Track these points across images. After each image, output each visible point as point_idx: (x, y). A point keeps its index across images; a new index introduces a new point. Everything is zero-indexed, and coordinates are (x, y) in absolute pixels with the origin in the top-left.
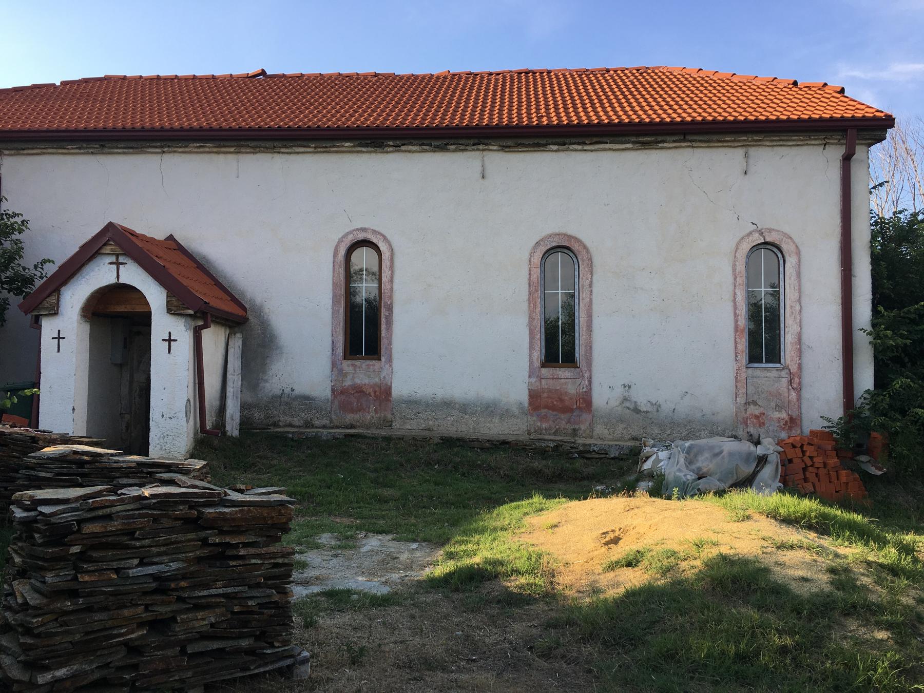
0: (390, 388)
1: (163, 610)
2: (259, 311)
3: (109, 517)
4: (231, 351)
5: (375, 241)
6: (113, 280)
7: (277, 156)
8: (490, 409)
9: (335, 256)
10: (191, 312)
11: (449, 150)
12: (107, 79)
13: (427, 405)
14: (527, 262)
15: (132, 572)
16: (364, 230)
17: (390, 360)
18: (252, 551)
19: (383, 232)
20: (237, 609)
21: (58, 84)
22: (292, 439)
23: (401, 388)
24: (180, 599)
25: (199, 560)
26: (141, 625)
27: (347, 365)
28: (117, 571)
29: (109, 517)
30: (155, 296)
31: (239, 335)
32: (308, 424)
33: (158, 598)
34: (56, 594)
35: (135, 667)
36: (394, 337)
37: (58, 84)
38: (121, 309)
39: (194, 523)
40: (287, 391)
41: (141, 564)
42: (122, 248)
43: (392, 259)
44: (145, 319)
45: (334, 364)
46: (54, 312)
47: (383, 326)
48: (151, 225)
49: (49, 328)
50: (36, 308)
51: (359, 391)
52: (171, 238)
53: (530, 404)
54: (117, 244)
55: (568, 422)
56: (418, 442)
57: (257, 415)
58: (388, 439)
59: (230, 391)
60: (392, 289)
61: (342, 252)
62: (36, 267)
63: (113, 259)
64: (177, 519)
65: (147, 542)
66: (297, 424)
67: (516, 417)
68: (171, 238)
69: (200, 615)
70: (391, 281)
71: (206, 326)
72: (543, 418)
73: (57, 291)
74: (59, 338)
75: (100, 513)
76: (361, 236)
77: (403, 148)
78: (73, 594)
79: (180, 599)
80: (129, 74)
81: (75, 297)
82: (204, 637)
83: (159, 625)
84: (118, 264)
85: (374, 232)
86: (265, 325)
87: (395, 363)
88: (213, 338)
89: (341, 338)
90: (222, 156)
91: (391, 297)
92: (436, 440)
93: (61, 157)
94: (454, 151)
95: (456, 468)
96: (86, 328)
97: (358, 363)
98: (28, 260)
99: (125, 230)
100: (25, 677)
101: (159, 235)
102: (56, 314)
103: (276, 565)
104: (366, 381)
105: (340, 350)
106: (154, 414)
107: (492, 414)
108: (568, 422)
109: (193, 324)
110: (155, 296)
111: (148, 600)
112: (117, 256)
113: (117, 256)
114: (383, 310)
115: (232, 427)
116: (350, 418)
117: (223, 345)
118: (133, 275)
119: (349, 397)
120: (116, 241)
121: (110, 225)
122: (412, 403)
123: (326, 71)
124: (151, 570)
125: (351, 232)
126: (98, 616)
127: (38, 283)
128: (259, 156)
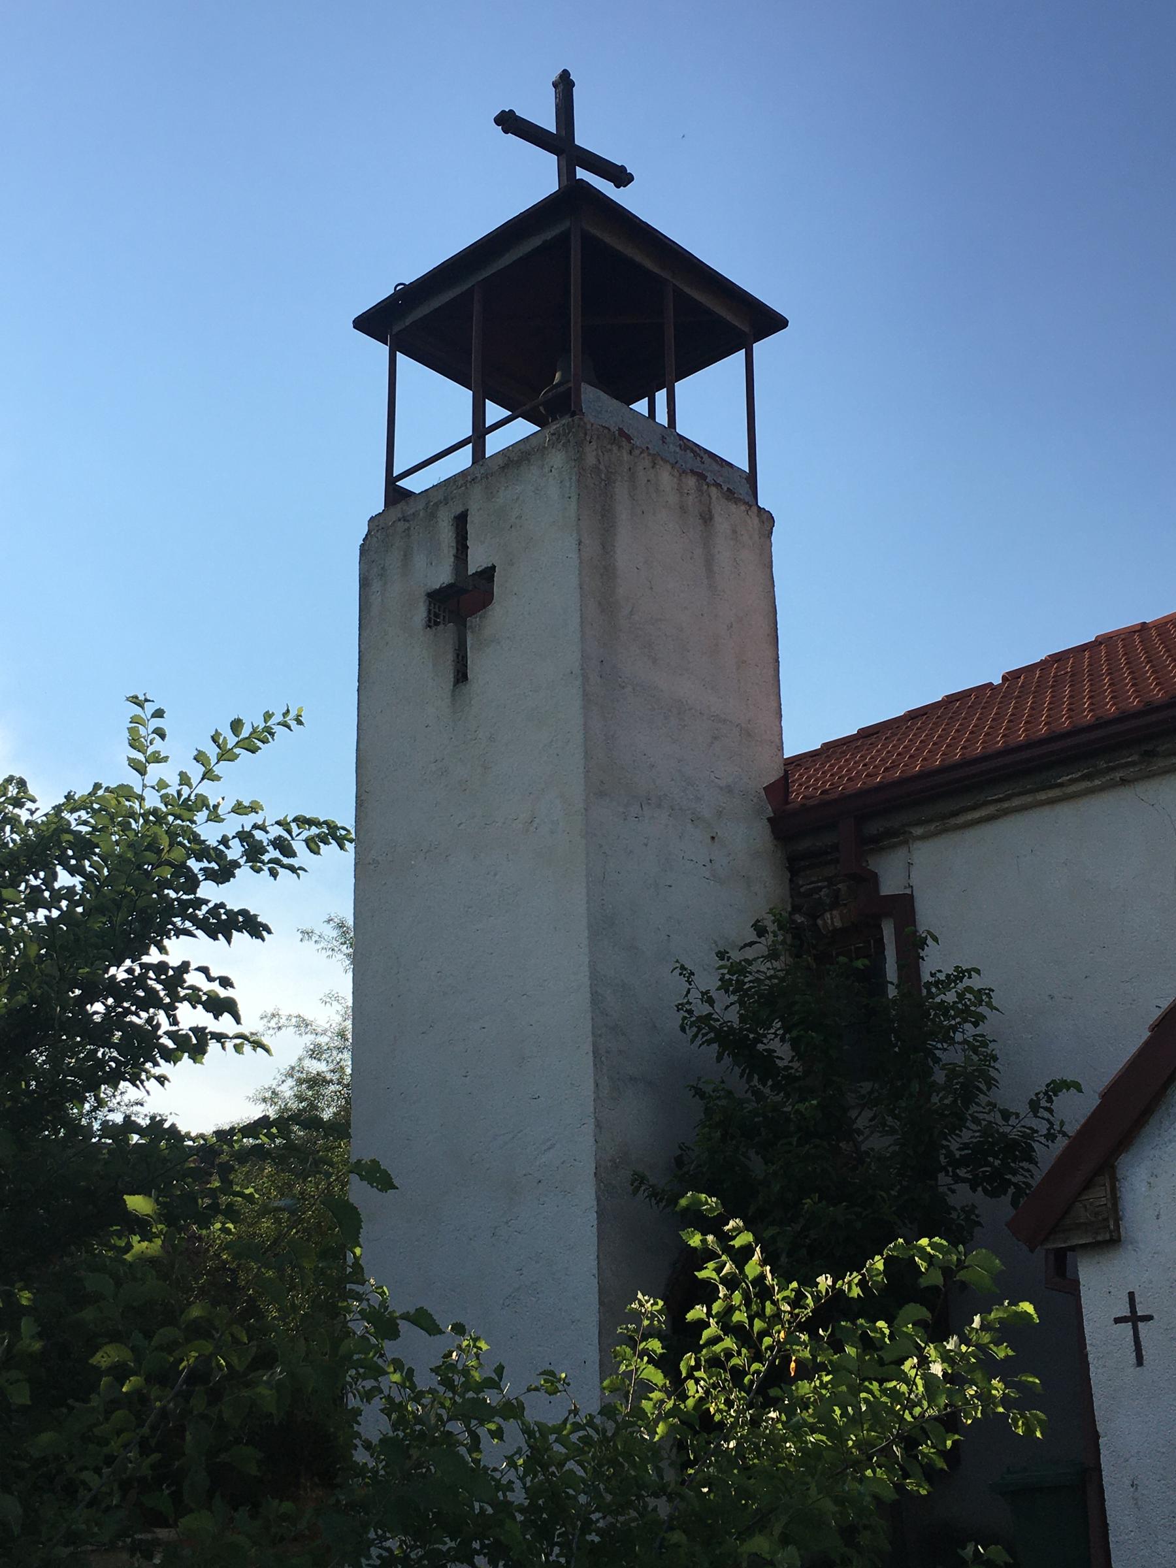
21: (997, 681)
37: (997, 681)
62: (1034, 1106)
98: (1013, 1090)
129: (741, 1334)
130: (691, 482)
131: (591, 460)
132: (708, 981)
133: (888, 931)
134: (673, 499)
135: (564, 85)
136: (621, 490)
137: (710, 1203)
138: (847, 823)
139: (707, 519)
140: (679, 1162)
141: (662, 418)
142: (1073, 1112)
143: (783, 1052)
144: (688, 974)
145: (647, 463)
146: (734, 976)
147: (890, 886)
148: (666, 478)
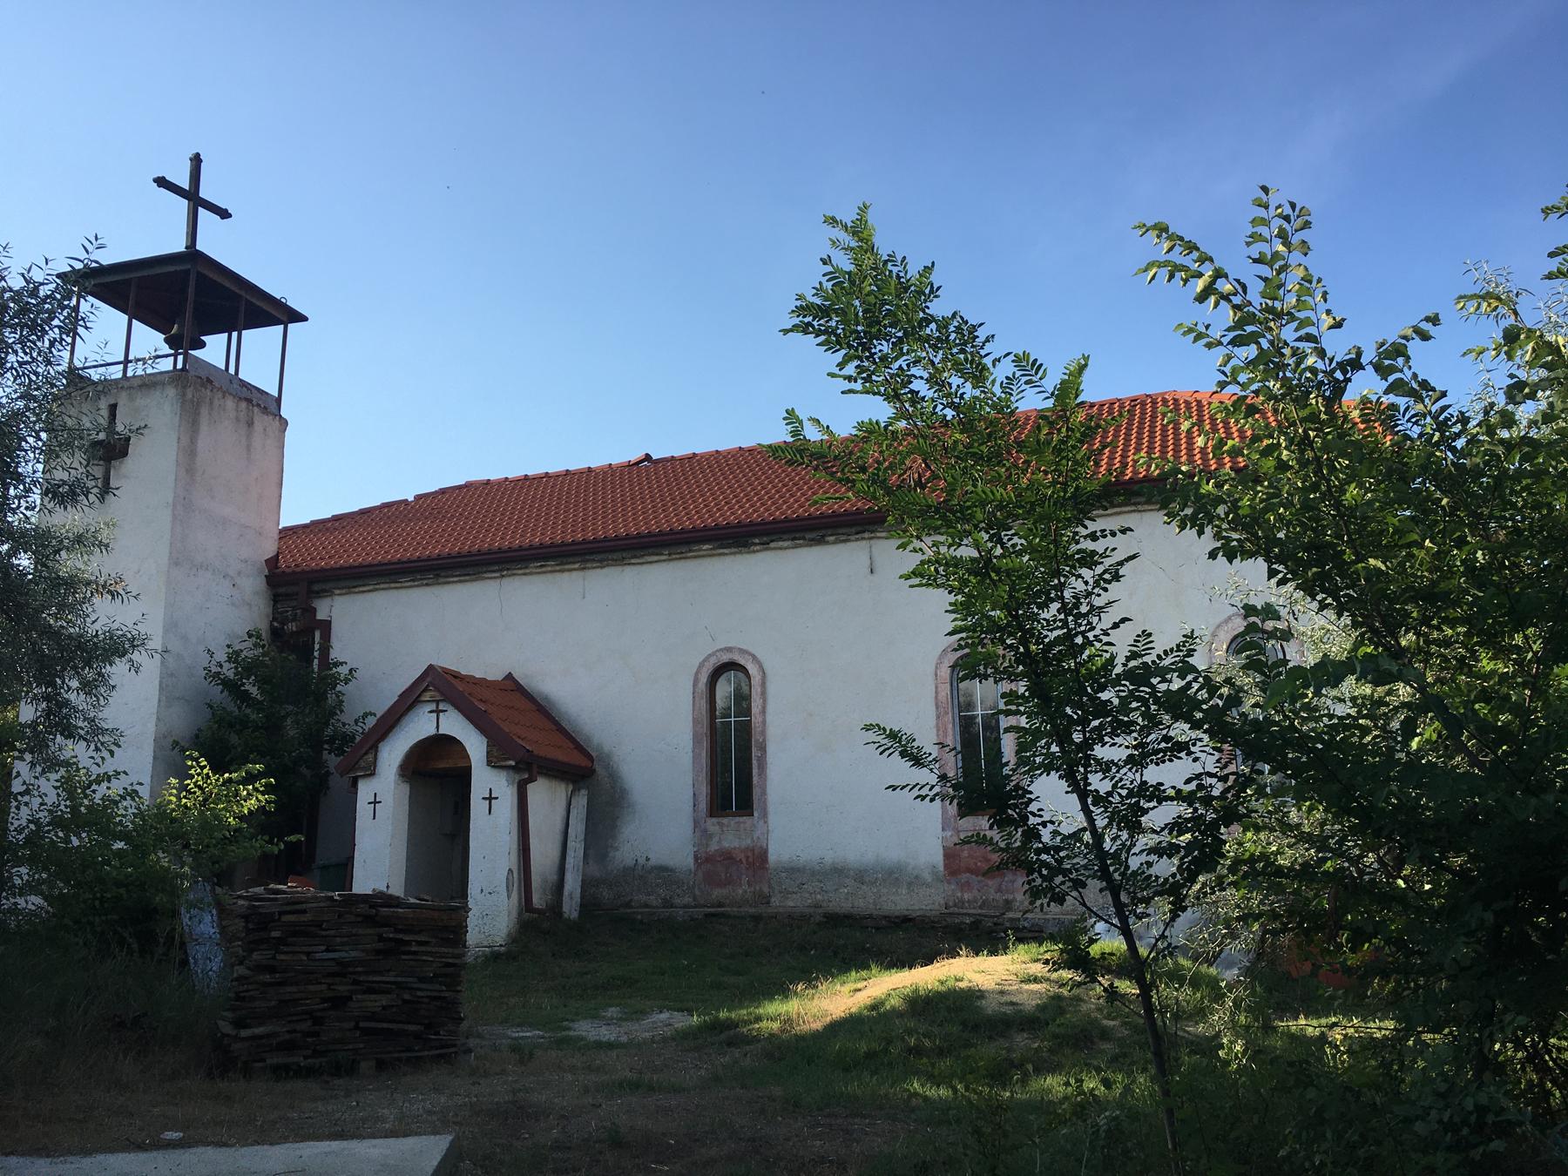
0: (766, 851)
1: (343, 989)
2: (606, 760)
3: (304, 912)
4: (573, 813)
5: (742, 662)
6: (432, 731)
7: (628, 569)
8: (893, 875)
9: (695, 685)
10: (512, 763)
11: (827, 543)
12: (468, 485)
13: (813, 873)
14: (931, 678)
15: (318, 956)
16: (729, 650)
17: (765, 815)
18: (423, 949)
19: (751, 650)
20: (407, 997)
21: (411, 499)
22: (641, 922)
23: (779, 852)
24: (355, 982)
25: (378, 952)
26: (324, 1000)
27: (712, 825)
28: (308, 954)
29: (304, 912)
30: (475, 746)
31: (584, 792)
32: (668, 904)
33: (337, 980)
34: (260, 968)
35: (317, 1034)
36: (769, 783)
37: (411, 499)
38: (442, 765)
39: (369, 920)
40: (642, 861)
41: (327, 951)
42: (442, 694)
43: (763, 684)
44: (463, 777)
45: (696, 823)
46: (371, 772)
47: (755, 771)
48: (482, 662)
49: (365, 791)
50: (353, 768)
51: (728, 857)
52: (509, 677)
53: (946, 866)
54: (437, 689)
55: (999, 890)
56: (797, 920)
57: (606, 894)
58: (757, 918)
59: (570, 861)
60: (764, 722)
61: (704, 679)
62: (356, 722)
63: (433, 706)
64: (358, 915)
65: (332, 932)
66: (654, 903)
67: (928, 885)
68: (509, 677)
69: (373, 997)
70: (763, 711)
71: (532, 780)
72: (967, 886)
73: (375, 748)
74: (375, 802)
75: (298, 907)
76: (725, 658)
77: (772, 545)
78: (272, 970)
79: (355, 982)
80: (493, 477)
81: (393, 753)
82: (373, 1017)
83: (339, 1002)
84: (438, 712)
85: (742, 651)
86: (614, 777)
87: (772, 818)
88: (546, 798)
89: (704, 790)
90: (566, 575)
91: (763, 733)
92: (818, 919)
93: (395, 592)
94: (834, 543)
95: (835, 954)
96: (406, 788)
97: (725, 821)
98: (348, 716)
99: (446, 671)
100: (234, 1033)
101: (495, 674)
102: (373, 774)
103: (448, 965)
104: (736, 844)
105: (703, 805)
106: (473, 889)
107: (897, 882)
108: (999, 890)
109: (517, 778)
110: (475, 746)
111: (329, 980)
112: (438, 702)
113: (438, 702)
114: (754, 750)
115: (571, 907)
116: (717, 893)
117: (564, 803)
118: (454, 725)
119: (714, 864)
120: (440, 685)
121: (431, 667)
122: (793, 870)
123: (723, 446)
124: (331, 955)
125: (713, 654)
126: (289, 989)
127: (358, 738)
128: (606, 570)
129: (200, 787)
130: (244, 405)
131: (189, 396)
132: (221, 656)
133: (317, 635)
134: (233, 414)
135: (197, 161)
136: (204, 411)
137: (196, 754)
138: (309, 577)
139: (250, 424)
140: (197, 736)
141: (232, 370)
142: (371, 722)
143: (254, 691)
144: (211, 654)
145: (220, 395)
146: (234, 657)
147: (320, 616)
148: (230, 403)
